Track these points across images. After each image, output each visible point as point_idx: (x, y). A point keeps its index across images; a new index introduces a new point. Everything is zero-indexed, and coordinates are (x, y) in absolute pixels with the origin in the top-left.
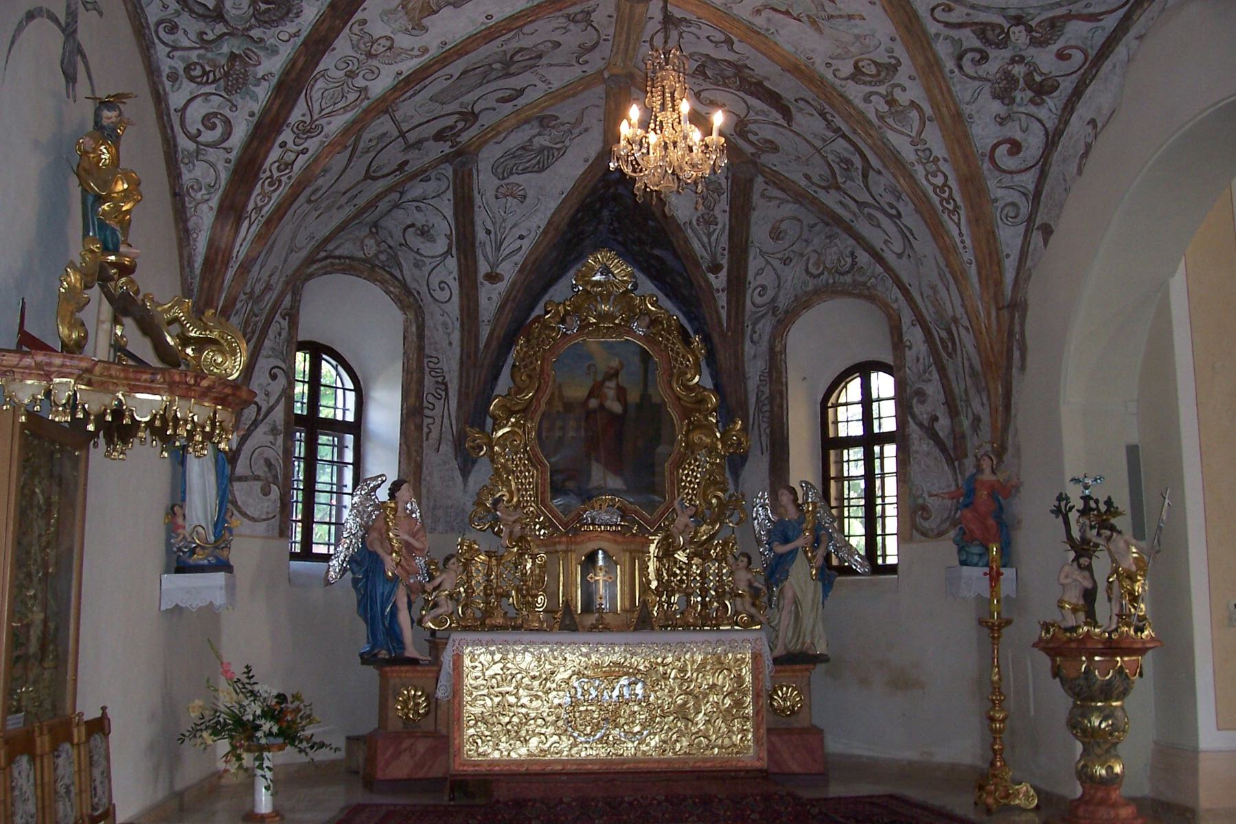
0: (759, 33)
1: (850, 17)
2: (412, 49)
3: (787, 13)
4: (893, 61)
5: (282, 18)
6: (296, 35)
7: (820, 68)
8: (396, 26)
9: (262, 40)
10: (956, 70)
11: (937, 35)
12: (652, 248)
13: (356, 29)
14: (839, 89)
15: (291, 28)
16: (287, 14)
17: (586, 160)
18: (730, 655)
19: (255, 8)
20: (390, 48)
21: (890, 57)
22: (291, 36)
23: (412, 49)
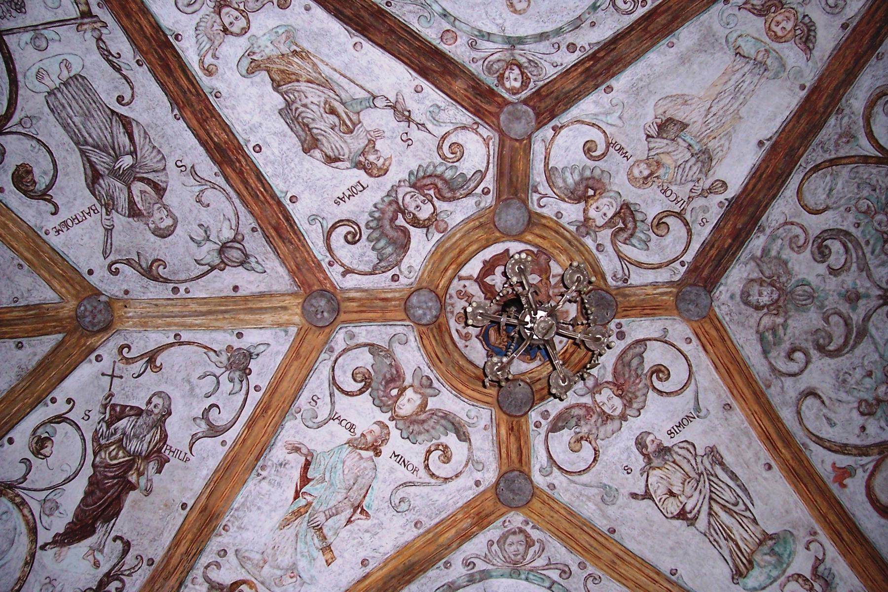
0: (257, 459)
1: (327, 548)
2: (214, 56)
3: (305, 480)
7: (214, 545)
8: (264, 41)
14: (189, 578)
17: (803, 87)
18: (323, 303)
20: (225, 31)
23: (214, 56)
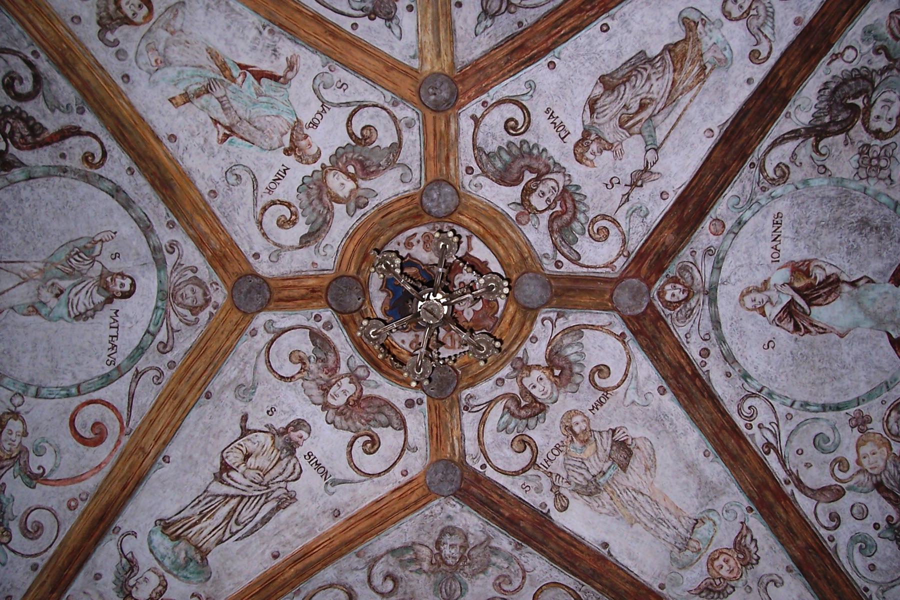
0: (281, 26)
3: (259, 75)
4: (110, 37)
5: (845, 82)
6: (836, 56)
9: (876, 52)
10: (31, 58)
11: (81, 111)
12: (423, 560)
13: (764, 49)
15: (839, 67)
16: (836, 89)
19: (869, 99)
21: (116, 43)
22: (842, 54)
